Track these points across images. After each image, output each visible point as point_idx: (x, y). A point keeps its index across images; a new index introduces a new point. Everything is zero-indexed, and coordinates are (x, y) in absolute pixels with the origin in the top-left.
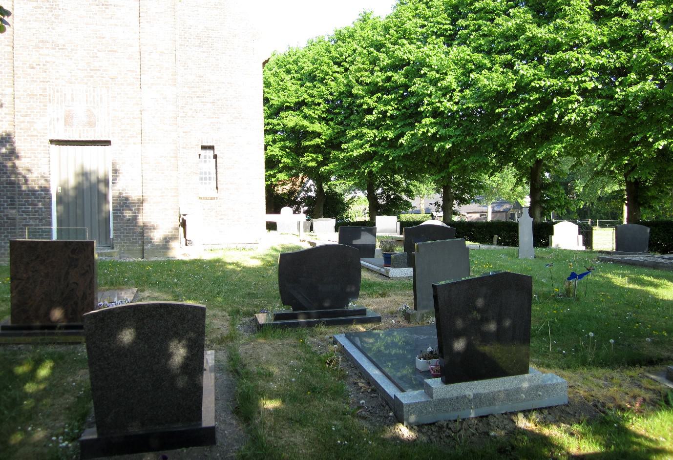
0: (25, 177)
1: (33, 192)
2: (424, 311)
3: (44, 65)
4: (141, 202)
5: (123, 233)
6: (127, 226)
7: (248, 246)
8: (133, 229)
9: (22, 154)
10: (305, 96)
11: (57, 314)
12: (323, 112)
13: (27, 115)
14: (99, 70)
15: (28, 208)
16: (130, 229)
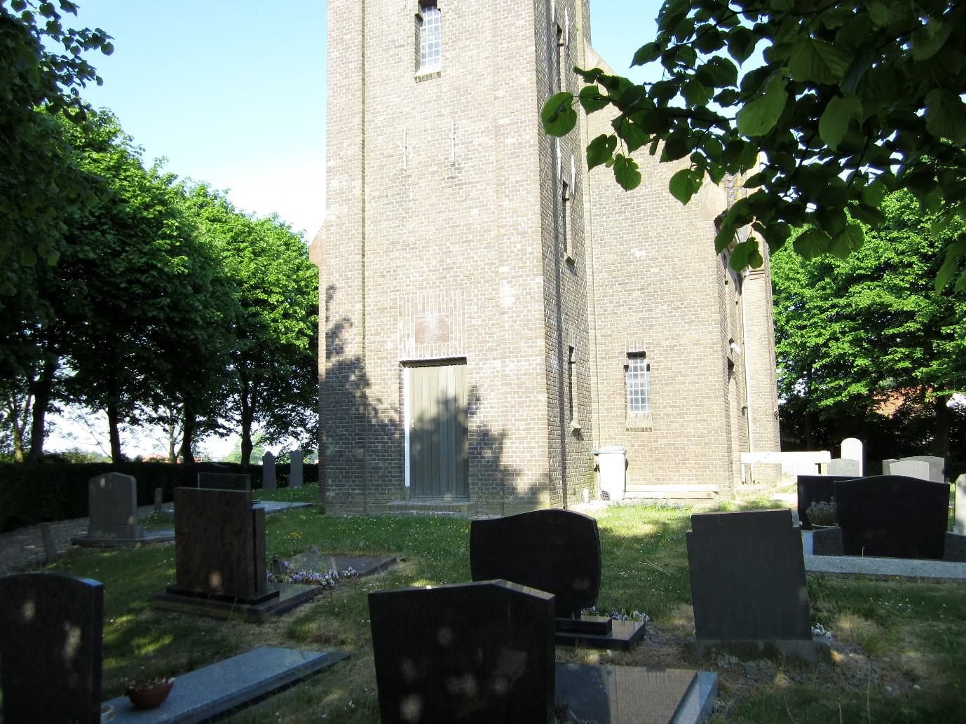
0: (375, 409)
1: (383, 426)
2: (711, 642)
3: (394, 271)
4: (503, 435)
5: (481, 479)
6: (485, 471)
7: (672, 503)
8: (493, 475)
9: (372, 381)
10: (890, 254)
11: (215, 580)
12: (921, 277)
13: (376, 334)
14: (452, 268)
15: (377, 447)
16: (488, 475)
